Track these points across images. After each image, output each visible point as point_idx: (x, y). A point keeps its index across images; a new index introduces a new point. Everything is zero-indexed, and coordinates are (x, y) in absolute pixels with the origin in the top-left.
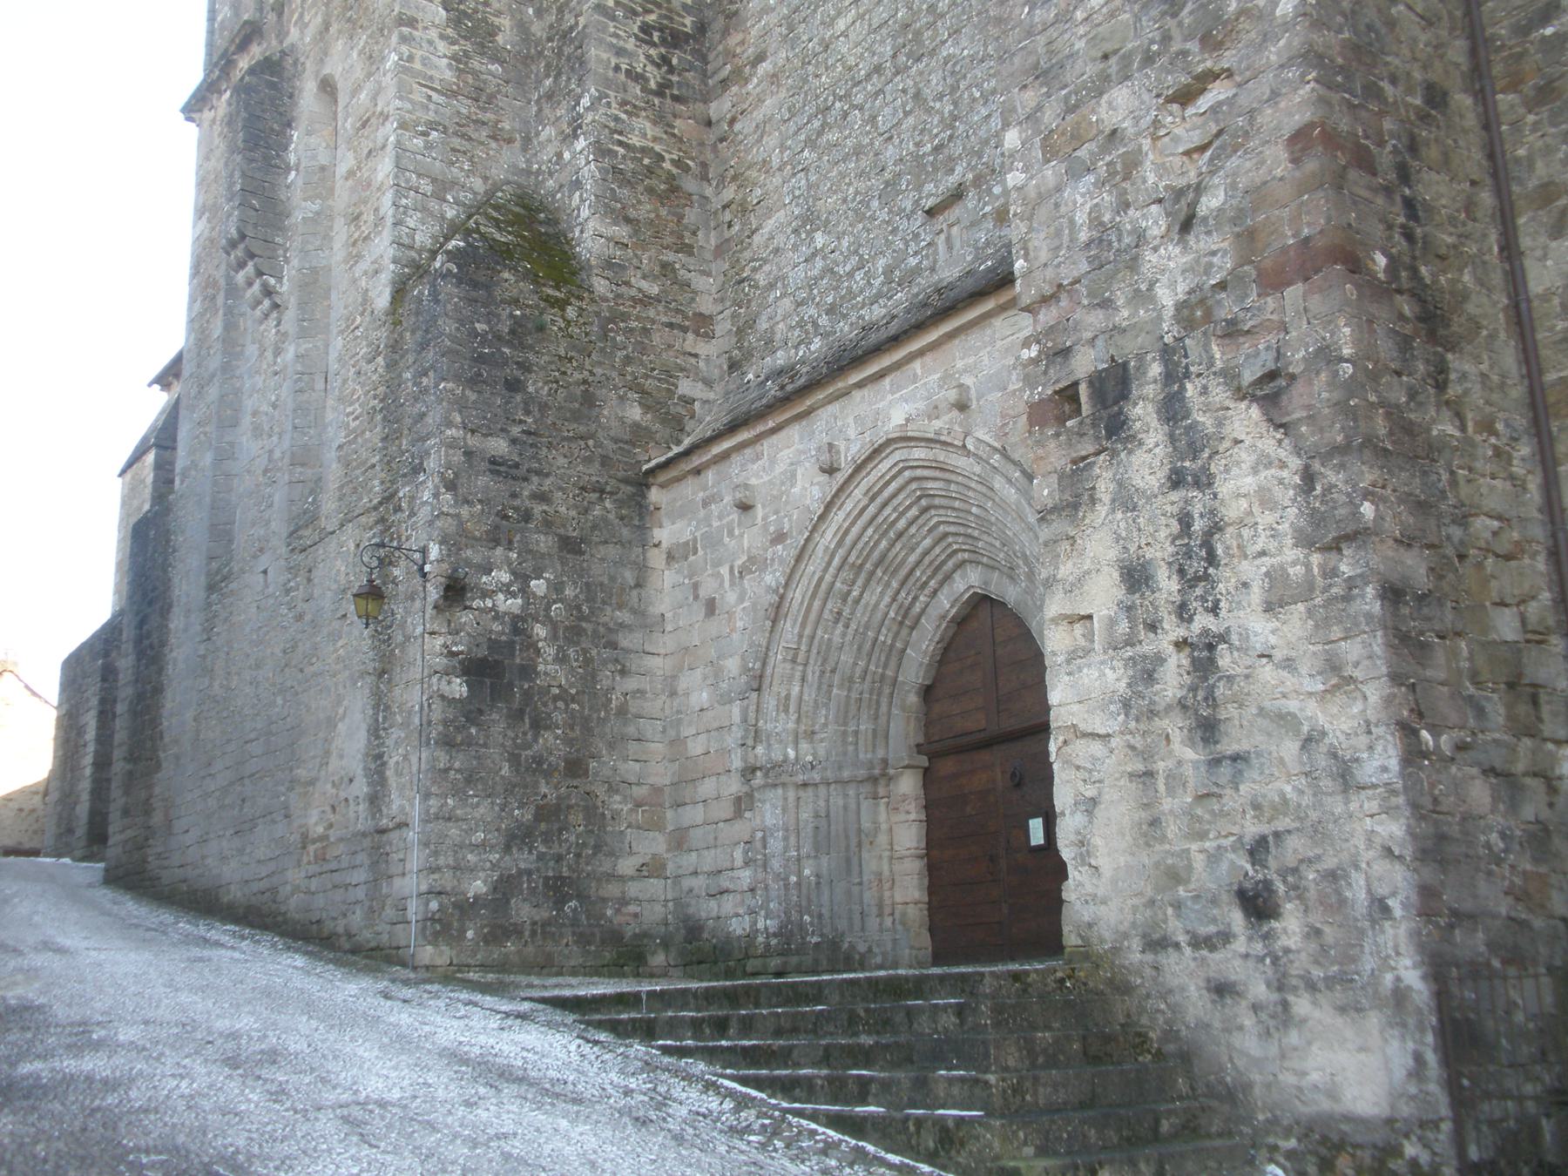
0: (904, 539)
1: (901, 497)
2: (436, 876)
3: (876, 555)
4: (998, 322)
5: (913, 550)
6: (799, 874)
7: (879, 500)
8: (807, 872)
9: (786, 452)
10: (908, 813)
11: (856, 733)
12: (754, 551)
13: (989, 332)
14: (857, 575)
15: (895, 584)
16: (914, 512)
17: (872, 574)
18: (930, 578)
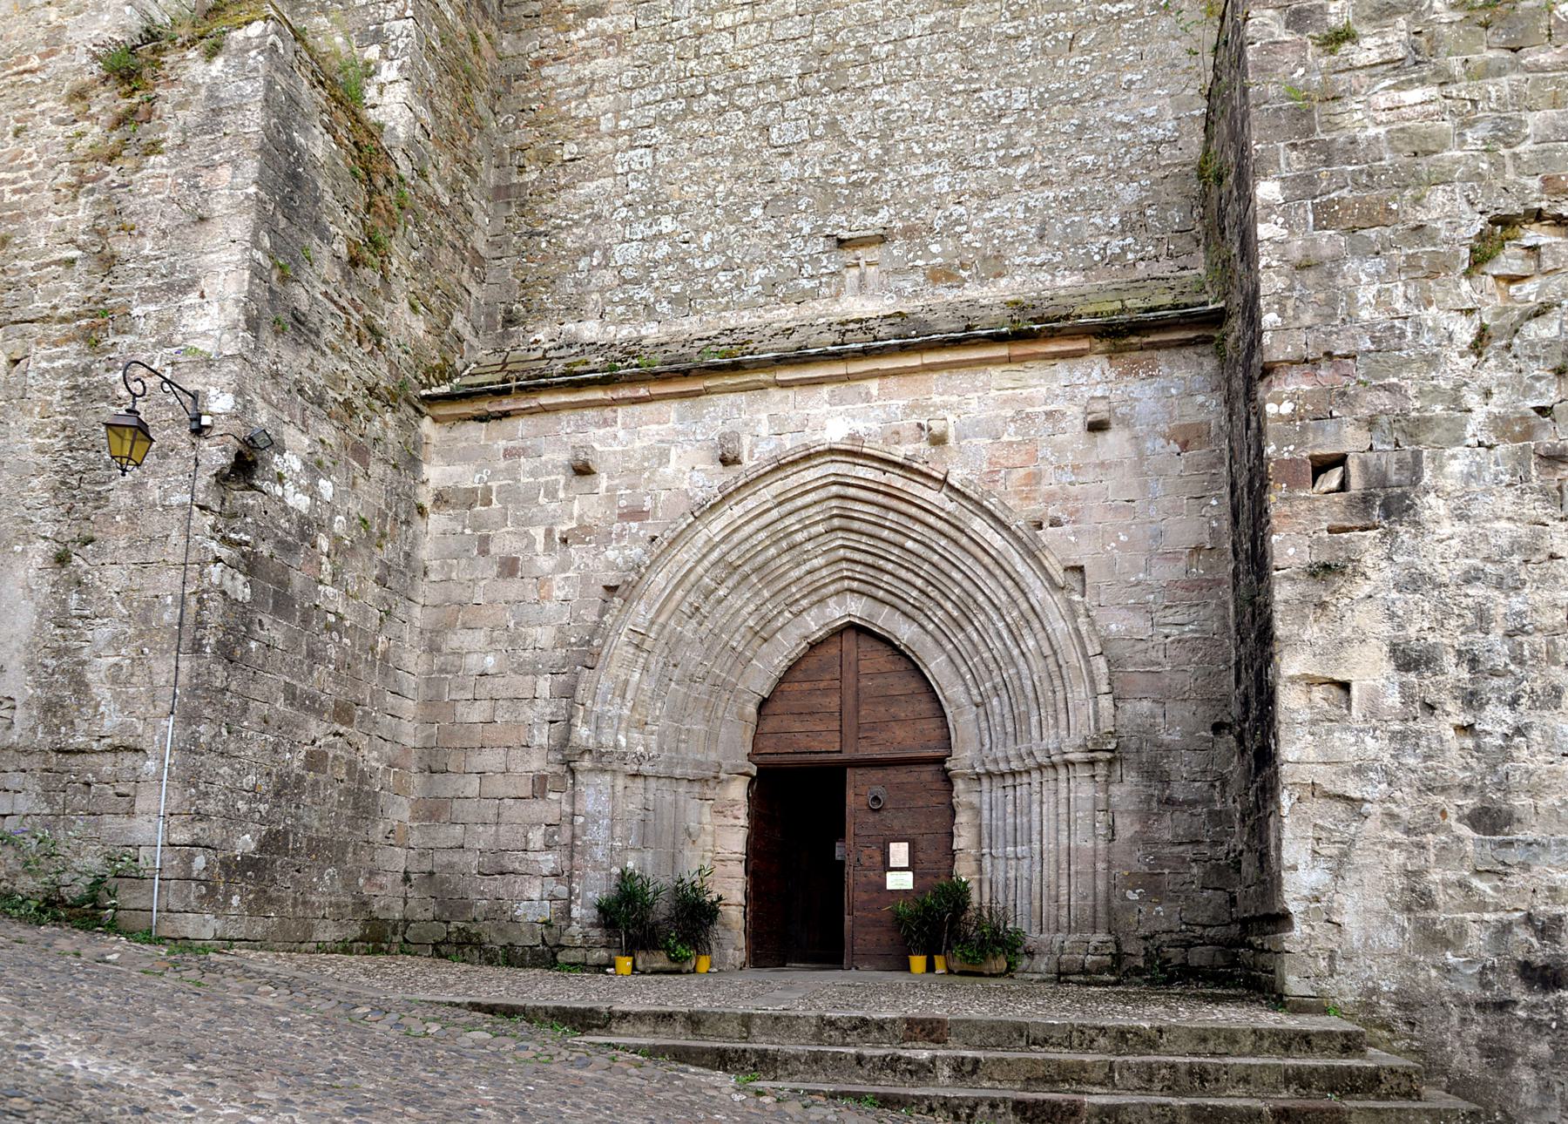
0: (795, 552)
1: (812, 511)
2: (204, 825)
3: (760, 559)
4: (995, 372)
5: (798, 565)
7: (788, 507)
9: (654, 427)
10: (737, 818)
12: (588, 521)
13: (982, 377)
15: (766, 594)
16: (821, 528)
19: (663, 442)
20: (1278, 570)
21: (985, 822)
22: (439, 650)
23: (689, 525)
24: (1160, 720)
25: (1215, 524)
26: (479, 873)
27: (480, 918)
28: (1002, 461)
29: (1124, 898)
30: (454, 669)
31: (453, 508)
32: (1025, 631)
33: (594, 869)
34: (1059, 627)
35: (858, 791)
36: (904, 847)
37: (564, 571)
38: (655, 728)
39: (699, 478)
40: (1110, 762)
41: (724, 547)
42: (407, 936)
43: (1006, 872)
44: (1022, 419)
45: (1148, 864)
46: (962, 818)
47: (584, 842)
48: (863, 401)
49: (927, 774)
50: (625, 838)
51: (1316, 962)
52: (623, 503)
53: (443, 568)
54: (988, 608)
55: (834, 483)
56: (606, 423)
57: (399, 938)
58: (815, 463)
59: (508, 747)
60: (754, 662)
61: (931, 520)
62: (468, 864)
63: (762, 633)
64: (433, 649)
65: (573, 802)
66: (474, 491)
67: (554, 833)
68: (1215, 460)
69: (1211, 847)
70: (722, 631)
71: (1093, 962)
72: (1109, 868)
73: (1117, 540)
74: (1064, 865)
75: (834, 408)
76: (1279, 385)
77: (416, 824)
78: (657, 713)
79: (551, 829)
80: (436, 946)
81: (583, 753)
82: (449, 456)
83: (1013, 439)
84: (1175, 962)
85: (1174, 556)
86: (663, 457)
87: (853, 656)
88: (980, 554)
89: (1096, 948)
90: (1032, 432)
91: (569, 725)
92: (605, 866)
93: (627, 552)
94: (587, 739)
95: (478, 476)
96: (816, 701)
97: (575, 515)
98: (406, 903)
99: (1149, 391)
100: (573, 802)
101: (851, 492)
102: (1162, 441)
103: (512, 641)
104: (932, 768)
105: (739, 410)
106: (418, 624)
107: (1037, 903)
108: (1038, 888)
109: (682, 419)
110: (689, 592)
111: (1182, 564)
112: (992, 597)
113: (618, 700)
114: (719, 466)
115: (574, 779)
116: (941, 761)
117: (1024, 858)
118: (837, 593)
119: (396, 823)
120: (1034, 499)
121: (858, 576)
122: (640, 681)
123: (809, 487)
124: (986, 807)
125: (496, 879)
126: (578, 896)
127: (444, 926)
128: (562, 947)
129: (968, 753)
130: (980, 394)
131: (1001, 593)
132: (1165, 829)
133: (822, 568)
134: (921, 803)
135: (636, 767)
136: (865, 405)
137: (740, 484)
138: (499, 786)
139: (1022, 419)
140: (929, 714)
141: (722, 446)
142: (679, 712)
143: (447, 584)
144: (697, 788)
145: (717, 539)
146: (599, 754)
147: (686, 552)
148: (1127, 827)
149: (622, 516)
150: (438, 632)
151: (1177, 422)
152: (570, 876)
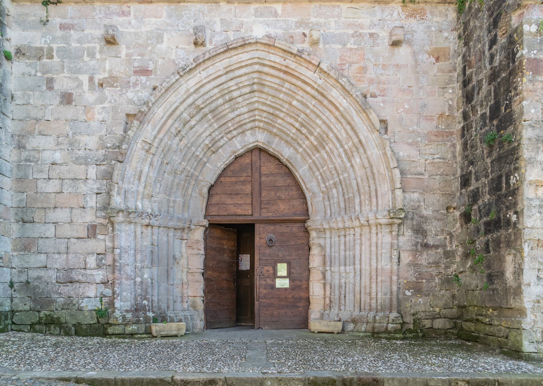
0: (232, 103)
1: (243, 79)
3: (214, 105)
5: (233, 111)
6: (142, 277)
8: (146, 276)
9: (153, 20)
10: (199, 250)
11: (175, 201)
12: (115, 74)
14: (198, 113)
15: (216, 126)
16: (247, 90)
17: (205, 115)
18: (235, 129)
19: (159, 29)
20: (525, 121)
21: (328, 253)
22: (24, 147)
23: (177, 80)
24: (422, 203)
25: (451, 103)
26: (57, 282)
27: (59, 309)
28: (347, 59)
29: (404, 294)
30: (35, 160)
31: (29, 59)
32: (355, 154)
33: (127, 279)
34: (374, 152)
35: (261, 236)
36: (285, 265)
37: (102, 103)
38: (156, 199)
39: (181, 52)
40: (399, 225)
41: (196, 96)
42: (14, 320)
43: (340, 279)
44: (357, 36)
45: (416, 277)
46: (315, 251)
47: (120, 264)
48: (273, 16)
49: (295, 228)
50: (142, 261)
51: (536, 334)
52: (136, 64)
53: (24, 96)
54: (335, 140)
55: (256, 63)
56: (123, 14)
57: (9, 321)
58: (248, 50)
59: (72, 208)
60: (207, 164)
61: (308, 89)
62: (50, 277)
63: (212, 149)
64: (21, 147)
65: (113, 239)
66: (41, 49)
67: (102, 259)
68: (452, 69)
69: (444, 269)
70: (192, 146)
71: (393, 327)
72: (398, 279)
73: (404, 107)
74: (374, 277)
75: (258, 19)
76: (528, 15)
77: (15, 254)
78: (158, 190)
79: (100, 256)
80: (32, 325)
81: (118, 212)
82: (23, 24)
83: (353, 47)
84: (427, 326)
85: (429, 118)
86: (159, 39)
87: (258, 164)
88: (334, 110)
89: (393, 320)
90: (363, 44)
91: (109, 194)
92: (133, 277)
93: (140, 94)
94: (120, 204)
95: (44, 40)
96: (238, 187)
97: (107, 69)
98: (12, 301)
99: (421, 27)
100: (113, 239)
101: (266, 69)
102: (427, 56)
103: (71, 144)
104: (298, 225)
105: (203, 14)
106: (10, 130)
107: (358, 296)
108: (359, 289)
109: (170, 16)
110: (175, 121)
111: (435, 123)
112: (338, 134)
113: (136, 182)
114: (193, 46)
115: (113, 227)
116: (304, 221)
117: (350, 272)
118: (251, 129)
119: (3, 253)
120: (363, 81)
121: (264, 119)
122: (149, 172)
123: (243, 64)
124: (328, 246)
125: (67, 286)
126: (118, 295)
127: (37, 314)
128: (111, 325)
129: (319, 218)
130: (336, 19)
131: (343, 131)
132: (425, 259)
133: (245, 113)
134: (293, 243)
135: (148, 221)
136: (274, 19)
137: (206, 58)
138: (66, 231)
139: (357, 36)
140: (296, 196)
141: (196, 34)
142: (169, 191)
143: (27, 107)
144: (179, 233)
145: (192, 90)
146: (128, 212)
147: (175, 97)
148: (406, 258)
149: (135, 72)
150: (23, 136)
151: (434, 46)
152: (113, 284)
